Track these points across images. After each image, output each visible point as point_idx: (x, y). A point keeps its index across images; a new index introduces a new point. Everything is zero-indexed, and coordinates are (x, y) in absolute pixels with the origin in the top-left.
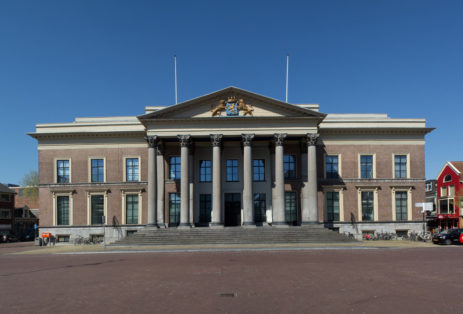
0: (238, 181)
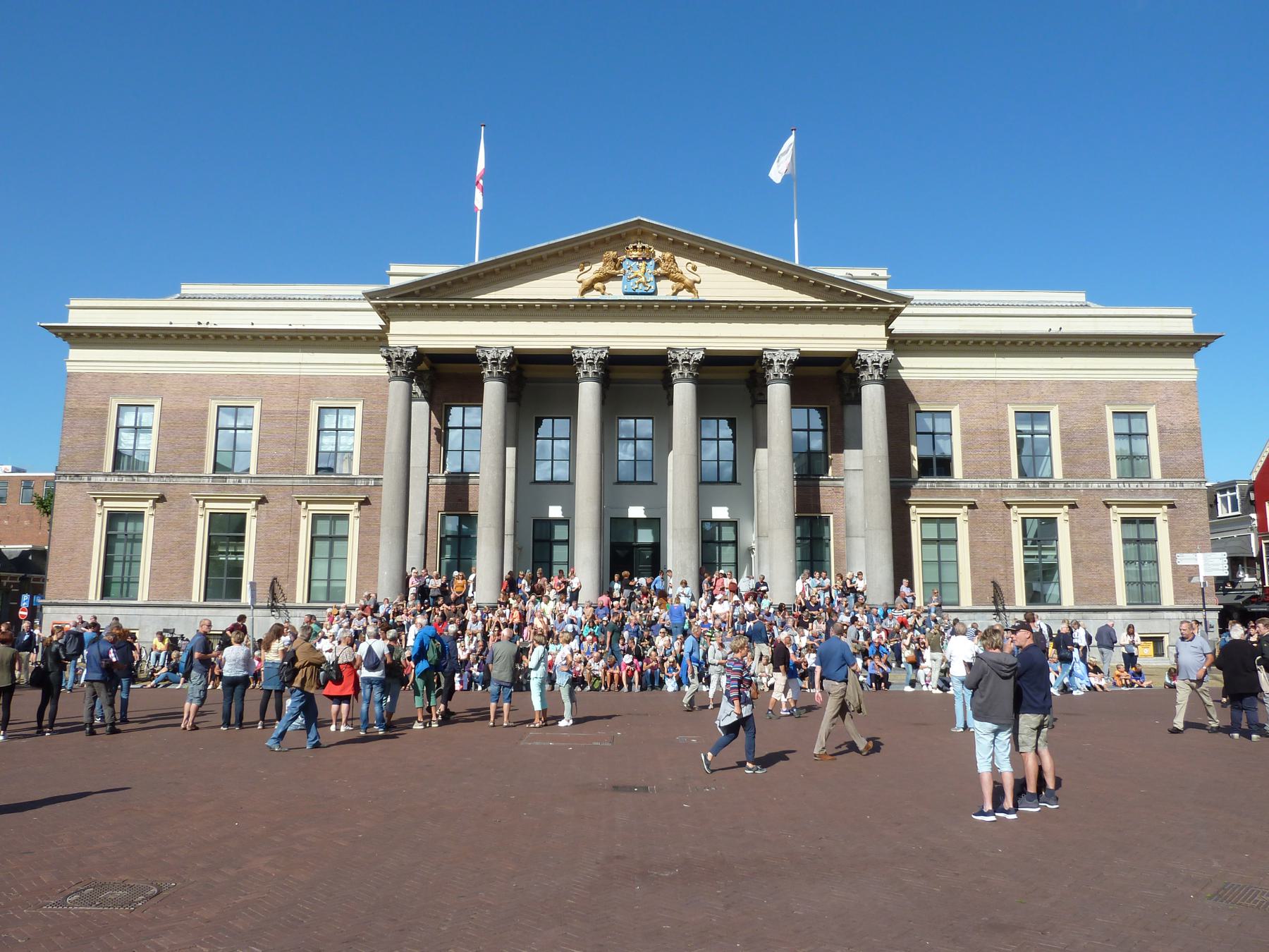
0: (651, 483)
